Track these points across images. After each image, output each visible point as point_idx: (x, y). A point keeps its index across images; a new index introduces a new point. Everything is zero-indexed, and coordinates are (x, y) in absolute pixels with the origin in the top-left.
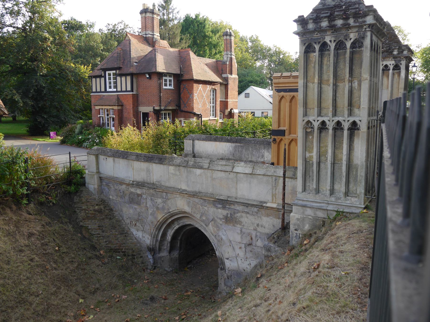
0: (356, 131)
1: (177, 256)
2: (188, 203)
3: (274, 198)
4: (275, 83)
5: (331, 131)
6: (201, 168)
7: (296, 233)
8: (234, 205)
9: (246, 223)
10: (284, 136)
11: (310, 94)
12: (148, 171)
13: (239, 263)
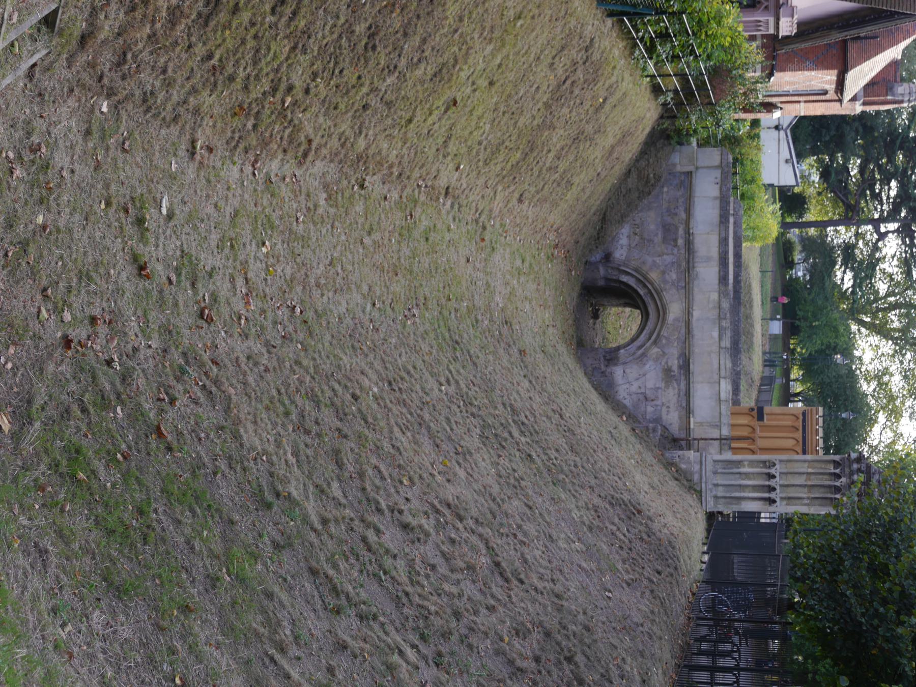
2: (676, 320)
5: (767, 483)
6: (720, 338)
11: (799, 464)
12: (709, 259)
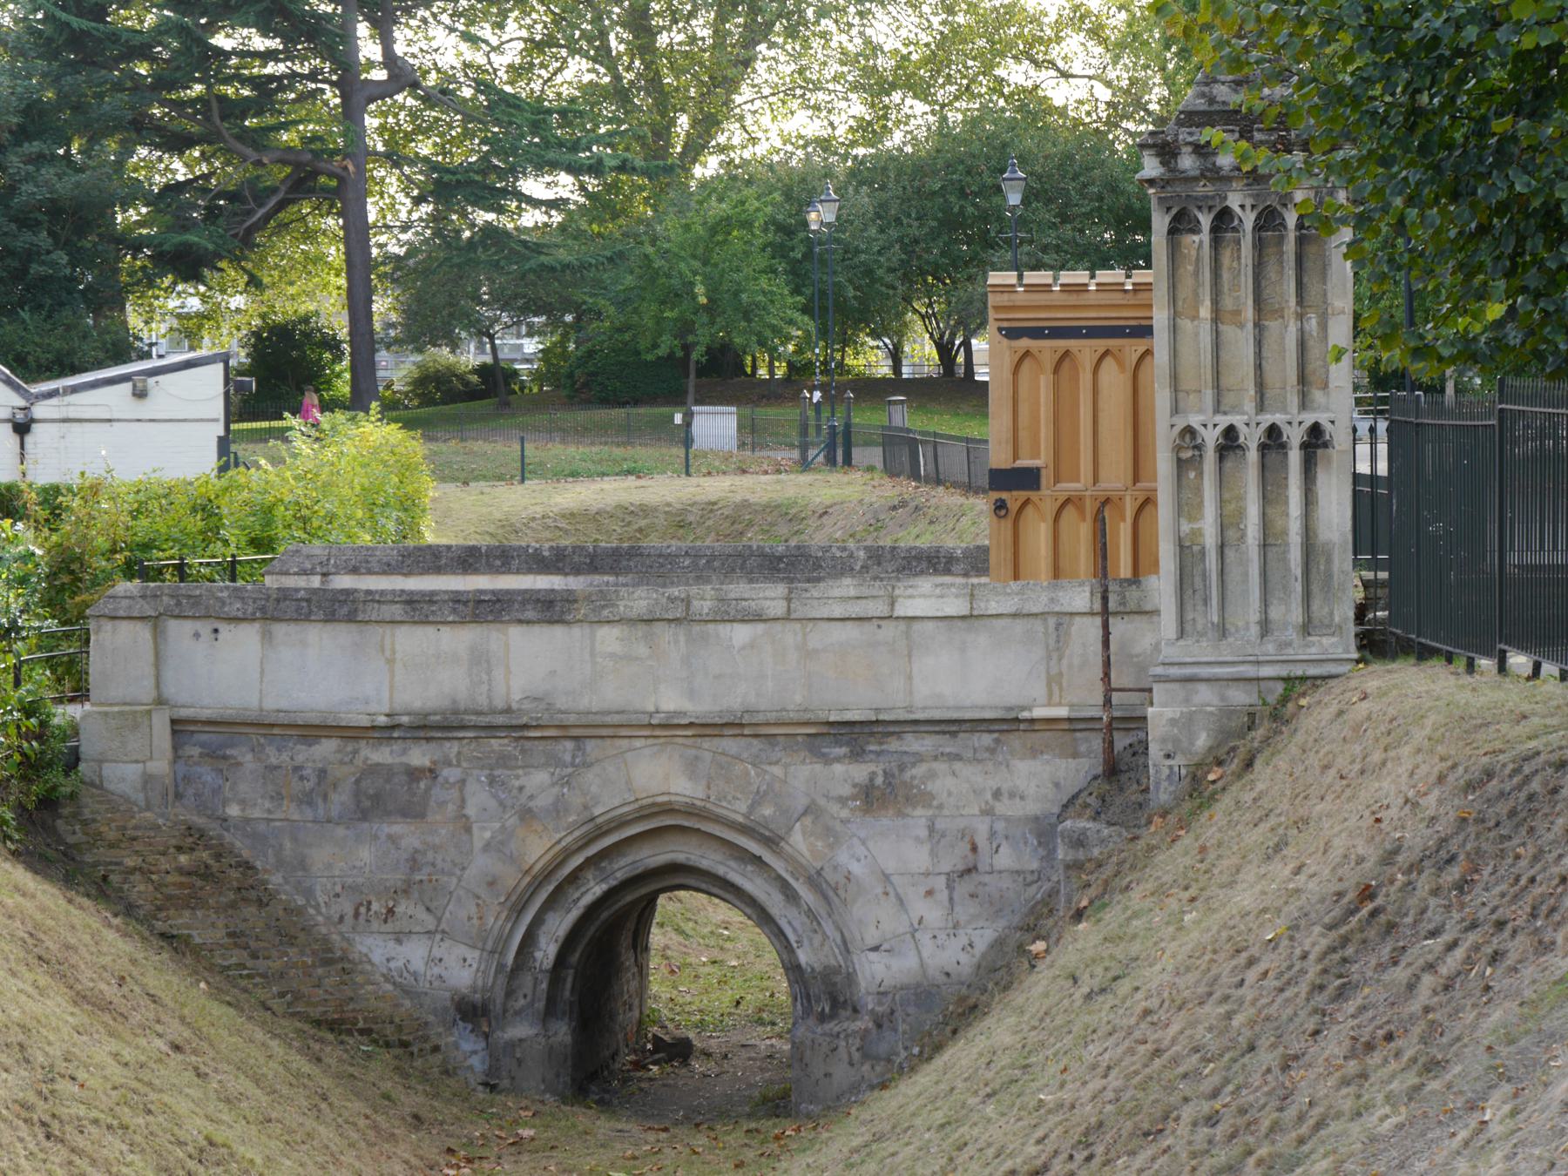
0: (1319, 452)
1: (568, 1039)
3: (1056, 689)
4: (996, 308)
5: (1253, 455)
7: (1171, 767)
8: (898, 735)
9: (950, 794)
10: (1038, 488)
11: (1185, 350)
13: (925, 954)
